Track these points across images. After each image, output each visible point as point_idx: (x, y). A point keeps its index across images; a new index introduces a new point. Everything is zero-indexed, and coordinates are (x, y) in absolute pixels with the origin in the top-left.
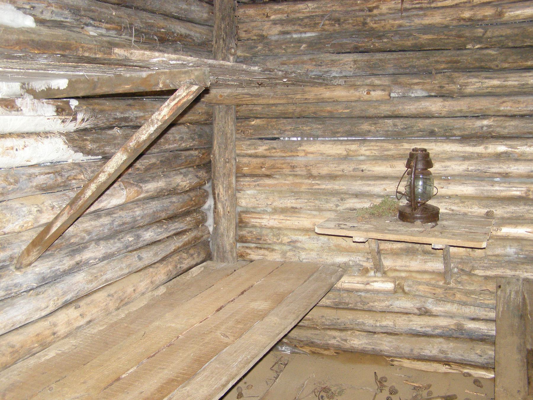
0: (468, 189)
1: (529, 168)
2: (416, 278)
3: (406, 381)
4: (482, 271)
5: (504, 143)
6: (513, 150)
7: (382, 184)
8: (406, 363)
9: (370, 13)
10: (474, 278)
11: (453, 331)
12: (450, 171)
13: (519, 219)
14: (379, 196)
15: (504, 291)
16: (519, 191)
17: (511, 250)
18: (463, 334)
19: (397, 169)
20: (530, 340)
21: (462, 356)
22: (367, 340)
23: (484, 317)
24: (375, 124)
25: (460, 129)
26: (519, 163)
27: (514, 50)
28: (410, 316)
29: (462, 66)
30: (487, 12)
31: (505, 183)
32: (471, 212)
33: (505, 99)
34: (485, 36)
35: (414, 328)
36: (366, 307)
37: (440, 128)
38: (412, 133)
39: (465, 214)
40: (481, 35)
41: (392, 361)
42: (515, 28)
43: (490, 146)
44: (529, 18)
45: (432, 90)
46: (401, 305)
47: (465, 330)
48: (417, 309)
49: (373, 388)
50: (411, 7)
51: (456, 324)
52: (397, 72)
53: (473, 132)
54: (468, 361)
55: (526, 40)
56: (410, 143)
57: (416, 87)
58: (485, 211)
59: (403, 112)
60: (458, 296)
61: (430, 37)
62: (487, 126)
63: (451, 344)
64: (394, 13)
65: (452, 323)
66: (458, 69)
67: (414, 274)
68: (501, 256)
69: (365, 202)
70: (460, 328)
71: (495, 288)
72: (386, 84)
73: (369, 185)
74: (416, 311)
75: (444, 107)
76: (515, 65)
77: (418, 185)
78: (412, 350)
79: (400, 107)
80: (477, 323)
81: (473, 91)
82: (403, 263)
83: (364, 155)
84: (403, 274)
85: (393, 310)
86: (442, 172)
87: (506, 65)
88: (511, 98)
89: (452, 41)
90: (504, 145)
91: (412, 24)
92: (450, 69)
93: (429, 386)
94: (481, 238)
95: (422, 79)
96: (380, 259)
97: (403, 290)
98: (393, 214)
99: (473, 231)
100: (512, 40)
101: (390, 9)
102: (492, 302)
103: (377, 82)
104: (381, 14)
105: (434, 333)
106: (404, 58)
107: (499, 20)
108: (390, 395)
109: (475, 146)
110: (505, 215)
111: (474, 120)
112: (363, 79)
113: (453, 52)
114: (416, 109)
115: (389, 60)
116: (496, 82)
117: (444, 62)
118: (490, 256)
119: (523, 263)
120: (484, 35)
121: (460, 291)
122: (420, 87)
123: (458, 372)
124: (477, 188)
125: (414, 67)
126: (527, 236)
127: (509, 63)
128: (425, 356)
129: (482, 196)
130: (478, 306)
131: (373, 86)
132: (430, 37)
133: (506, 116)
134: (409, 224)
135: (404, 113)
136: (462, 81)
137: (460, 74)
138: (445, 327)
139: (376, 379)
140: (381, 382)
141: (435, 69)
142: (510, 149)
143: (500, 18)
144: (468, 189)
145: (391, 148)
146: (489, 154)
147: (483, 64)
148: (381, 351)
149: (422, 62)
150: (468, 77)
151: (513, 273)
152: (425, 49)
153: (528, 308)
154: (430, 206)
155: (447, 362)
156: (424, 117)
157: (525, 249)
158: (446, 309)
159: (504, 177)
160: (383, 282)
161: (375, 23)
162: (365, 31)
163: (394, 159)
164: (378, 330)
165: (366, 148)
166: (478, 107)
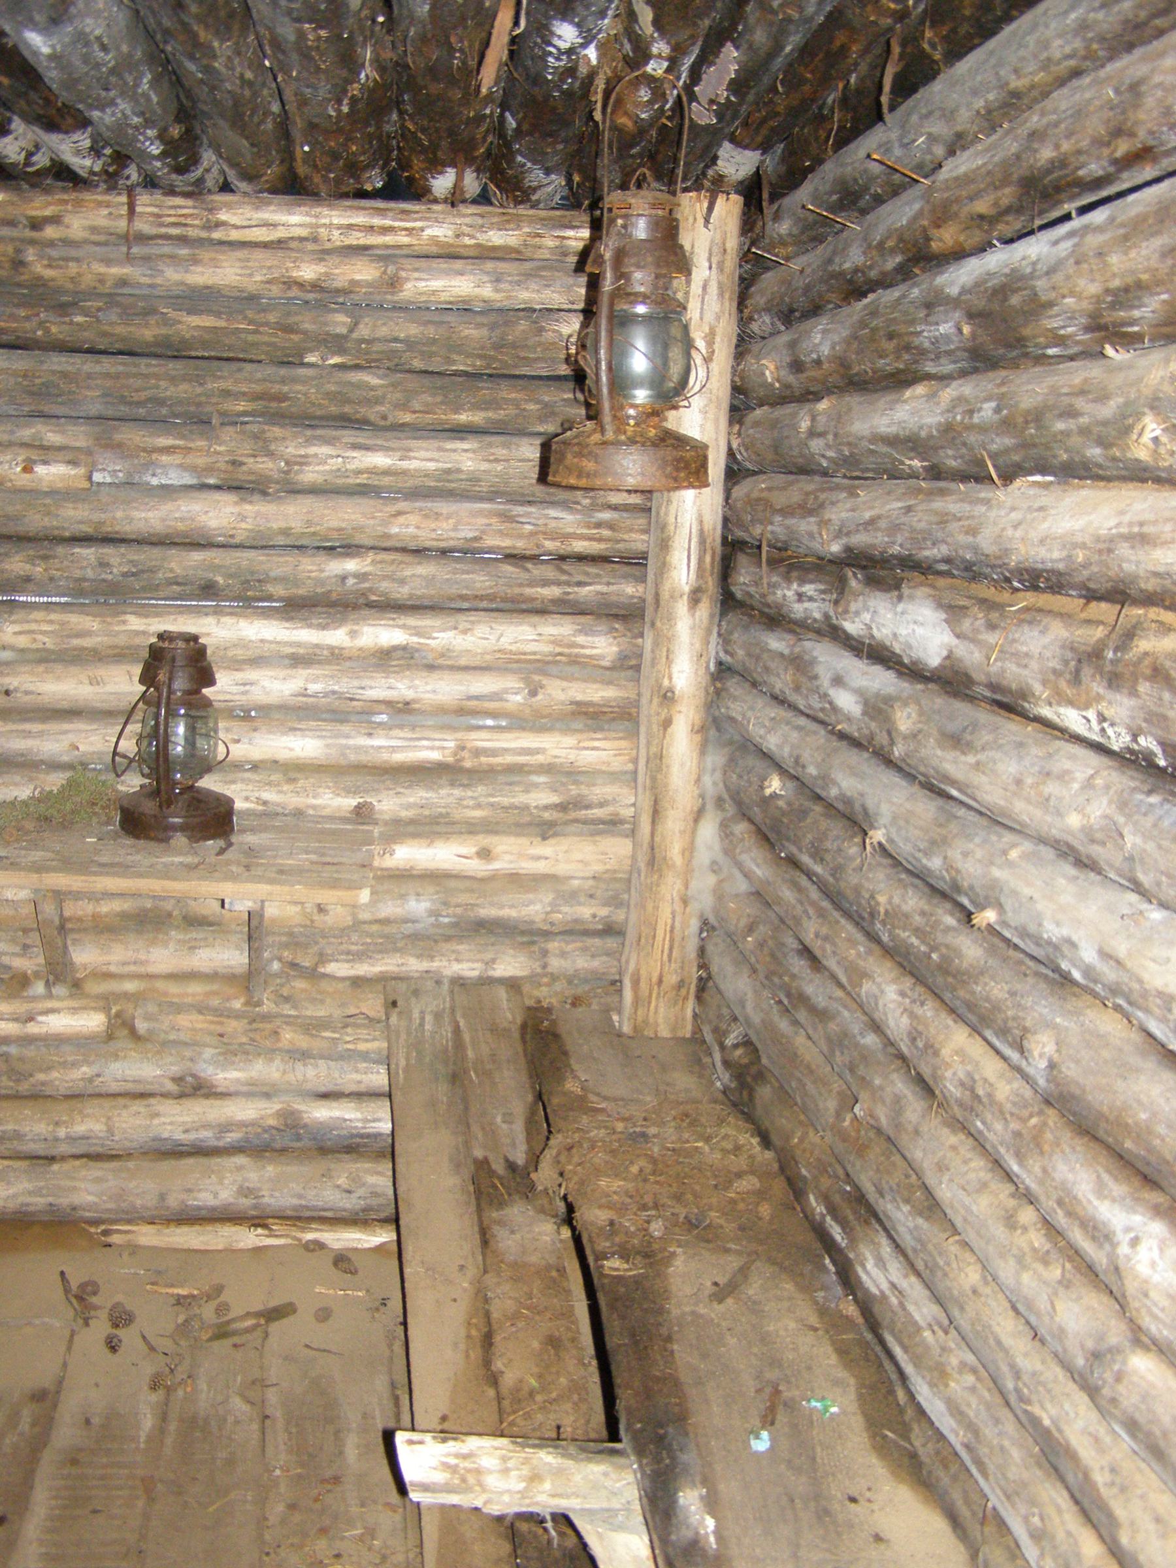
0: (304, 746)
1: (463, 688)
2: (166, 994)
3: (153, 1284)
4: (346, 965)
5: (401, 622)
6: (422, 641)
7: (66, 732)
8: (145, 1234)
9: (34, 234)
10: (324, 985)
11: (274, 1132)
12: (258, 695)
13: (438, 824)
14: (55, 766)
15: (406, 1014)
16: (439, 748)
17: (418, 906)
18: (299, 1138)
19: (110, 688)
20: (480, 1136)
21: (300, 1197)
22: (30, 1181)
23: (353, 1088)
24: (45, 558)
25: (282, 580)
26: (436, 675)
27: (427, 381)
28: (152, 1101)
29: (293, 410)
30: (360, 271)
31: (401, 727)
32: (314, 807)
33: (402, 505)
34: (355, 335)
35: (166, 1135)
36: (24, 1087)
37: (231, 576)
38: (152, 589)
39: (299, 813)
40: (344, 331)
41: (106, 1233)
42: (430, 322)
43: (366, 629)
44: (464, 302)
45: (209, 469)
46: (128, 1072)
47: (305, 1126)
48: (174, 1079)
49: (60, 1319)
50: (154, 231)
51: (279, 1114)
52: (110, 413)
53: (319, 590)
54: (315, 1209)
55: (455, 357)
56: (147, 616)
57: (165, 459)
58: (353, 802)
59: (127, 528)
60: (288, 1036)
61: (208, 321)
62: (356, 575)
63: (270, 1168)
64: (106, 244)
65: (269, 1112)
66: (283, 416)
67: (160, 985)
68: (395, 921)
69: (16, 784)
70: (291, 1122)
71: (383, 1010)
72: (78, 444)
73: (28, 734)
74: (171, 1087)
75: (243, 518)
76: (429, 417)
77: (177, 735)
78: (162, 1197)
79: (119, 514)
80: (335, 1104)
81: (320, 479)
82: (130, 955)
83: (12, 648)
84: (130, 986)
85: (103, 1090)
86: (237, 697)
87: (408, 418)
88: (417, 504)
89: (266, 339)
90: (398, 626)
91: (159, 281)
92: (262, 414)
93: (219, 1289)
94: (355, 877)
95: (183, 437)
96: (65, 947)
97: (134, 1034)
98: (104, 818)
99: (328, 859)
100: (422, 353)
101: (94, 229)
102: (376, 1045)
103: (53, 437)
104: (67, 242)
105: (221, 1144)
106: (135, 376)
107: (389, 297)
108: (115, 1331)
109: (323, 627)
110: (404, 814)
111: (321, 558)
112: (9, 427)
113: (270, 370)
114: (163, 520)
115: (89, 376)
116: (380, 460)
117: (244, 394)
118: (365, 922)
119: (448, 939)
120: (351, 331)
121: (289, 1021)
122: (177, 459)
123: (289, 1241)
124: (330, 741)
125: (161, 402)
126: (458, 867)
127: (415, 412)
128: (199, 1208)
129: (343, 762)
130: (341, 1057)
131: (42, 447)
132: (208, 321)
133: (404, 550)
134: (152, 844)
135: (127, 529)
136: (292, 449)
137: (287, 432)
138: (253, 1124)
139: (67, 1291)
140: (82, 1298)
141: (223, 414)
142: (415, 639)
143: (393, 294)
144: (304, 746)
145: (91, 628)
146: (360, 649)
147: (347, 409)
148: (74, 1209)
149: (183, 390)
150: (309, 442)
151: (425, 965)
152: (193, 354)
153: (470, 1053)
154: (209, 793)
155: (258, 1220)
156: (185, 544)
157: (454, 901)
158: (254, 1074)
159: (400, 711)
160: (74, 1011)
161: (50, 266)
162: (19, 285)
163: (100, 660)
164: (64, 1149)
165: (17, 628)
166: (335, 524)
